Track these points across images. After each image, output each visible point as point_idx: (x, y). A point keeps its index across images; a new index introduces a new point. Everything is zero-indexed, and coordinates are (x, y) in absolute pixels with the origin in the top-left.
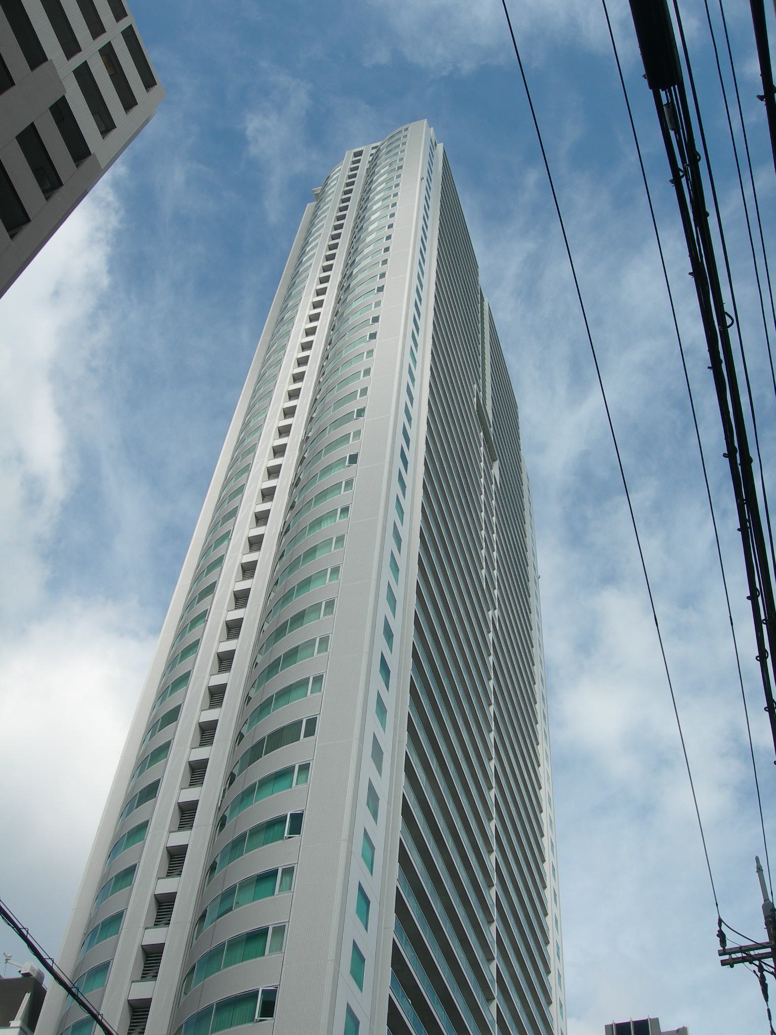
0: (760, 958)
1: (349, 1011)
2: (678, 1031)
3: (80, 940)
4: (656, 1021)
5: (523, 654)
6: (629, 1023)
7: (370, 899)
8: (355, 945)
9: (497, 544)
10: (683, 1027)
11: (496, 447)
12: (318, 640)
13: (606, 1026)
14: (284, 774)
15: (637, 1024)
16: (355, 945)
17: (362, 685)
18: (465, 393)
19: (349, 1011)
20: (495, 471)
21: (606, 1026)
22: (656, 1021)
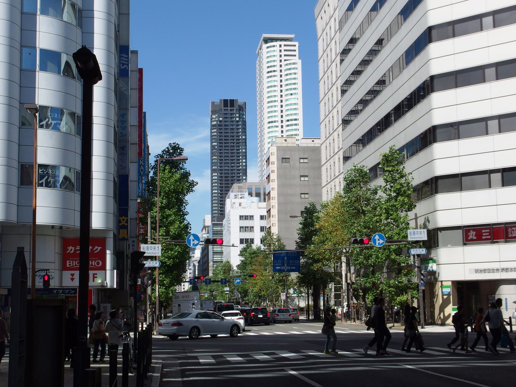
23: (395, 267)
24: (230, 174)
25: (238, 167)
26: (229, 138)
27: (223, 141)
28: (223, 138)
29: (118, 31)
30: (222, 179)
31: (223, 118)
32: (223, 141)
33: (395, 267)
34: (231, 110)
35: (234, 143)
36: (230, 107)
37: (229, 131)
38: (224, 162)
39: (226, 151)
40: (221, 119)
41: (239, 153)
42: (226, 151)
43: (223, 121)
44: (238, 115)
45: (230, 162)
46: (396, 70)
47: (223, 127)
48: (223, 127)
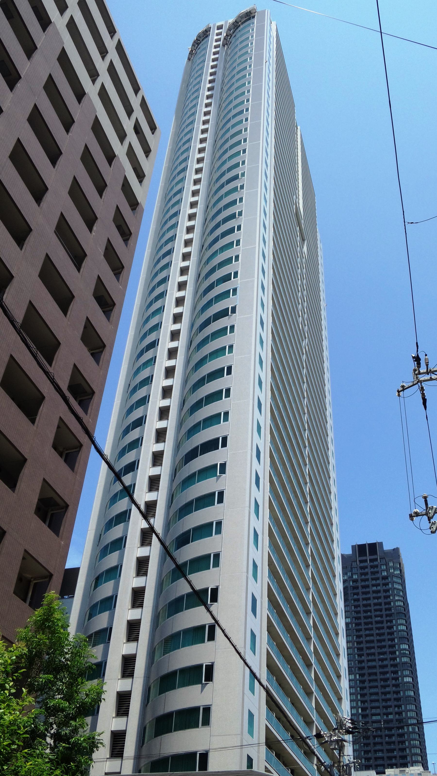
0: (427, 373)
1: (250, 712)
2: (394, 549)
3: (200, 231)
4: (381, 544)
5: (317, 341)
6: (365, 545)
7: (257, 564)
8: (251, 630)
9: (307, 309)
10: (397, 548)
11: (306, 235)
12: (238, 199)
13: (352, 546)
14: (231, 245)
15: (370, 545)
16: (251, 630)
17: (252, 372)
18: (293, 228)
19: (250, 712)
20: (305, 249)
21: (352, 546)
22: (381, 544)
23: (69, 663)
24: (378, 674)
25: (394, 661)
26: (378, 670)
27: (362, 609)
28: (362, 621)
29: (297, 198)
30: (361, 653)
31: (359, 574)
32: (362, 609)
33: (69, 663)
34: (371, 561)
35: (381, 616)
36: (370, 555)
37: (371, 595)
38: (362, 621)
39: (368, 632)
40: (355, 577)
41: (387, 591)
42: (368, 632)
43: (359, 580)
44: (385, 567)
45: (379, 684)
46: (212, 198)
47: (360, 590)
48: (360, 590)
